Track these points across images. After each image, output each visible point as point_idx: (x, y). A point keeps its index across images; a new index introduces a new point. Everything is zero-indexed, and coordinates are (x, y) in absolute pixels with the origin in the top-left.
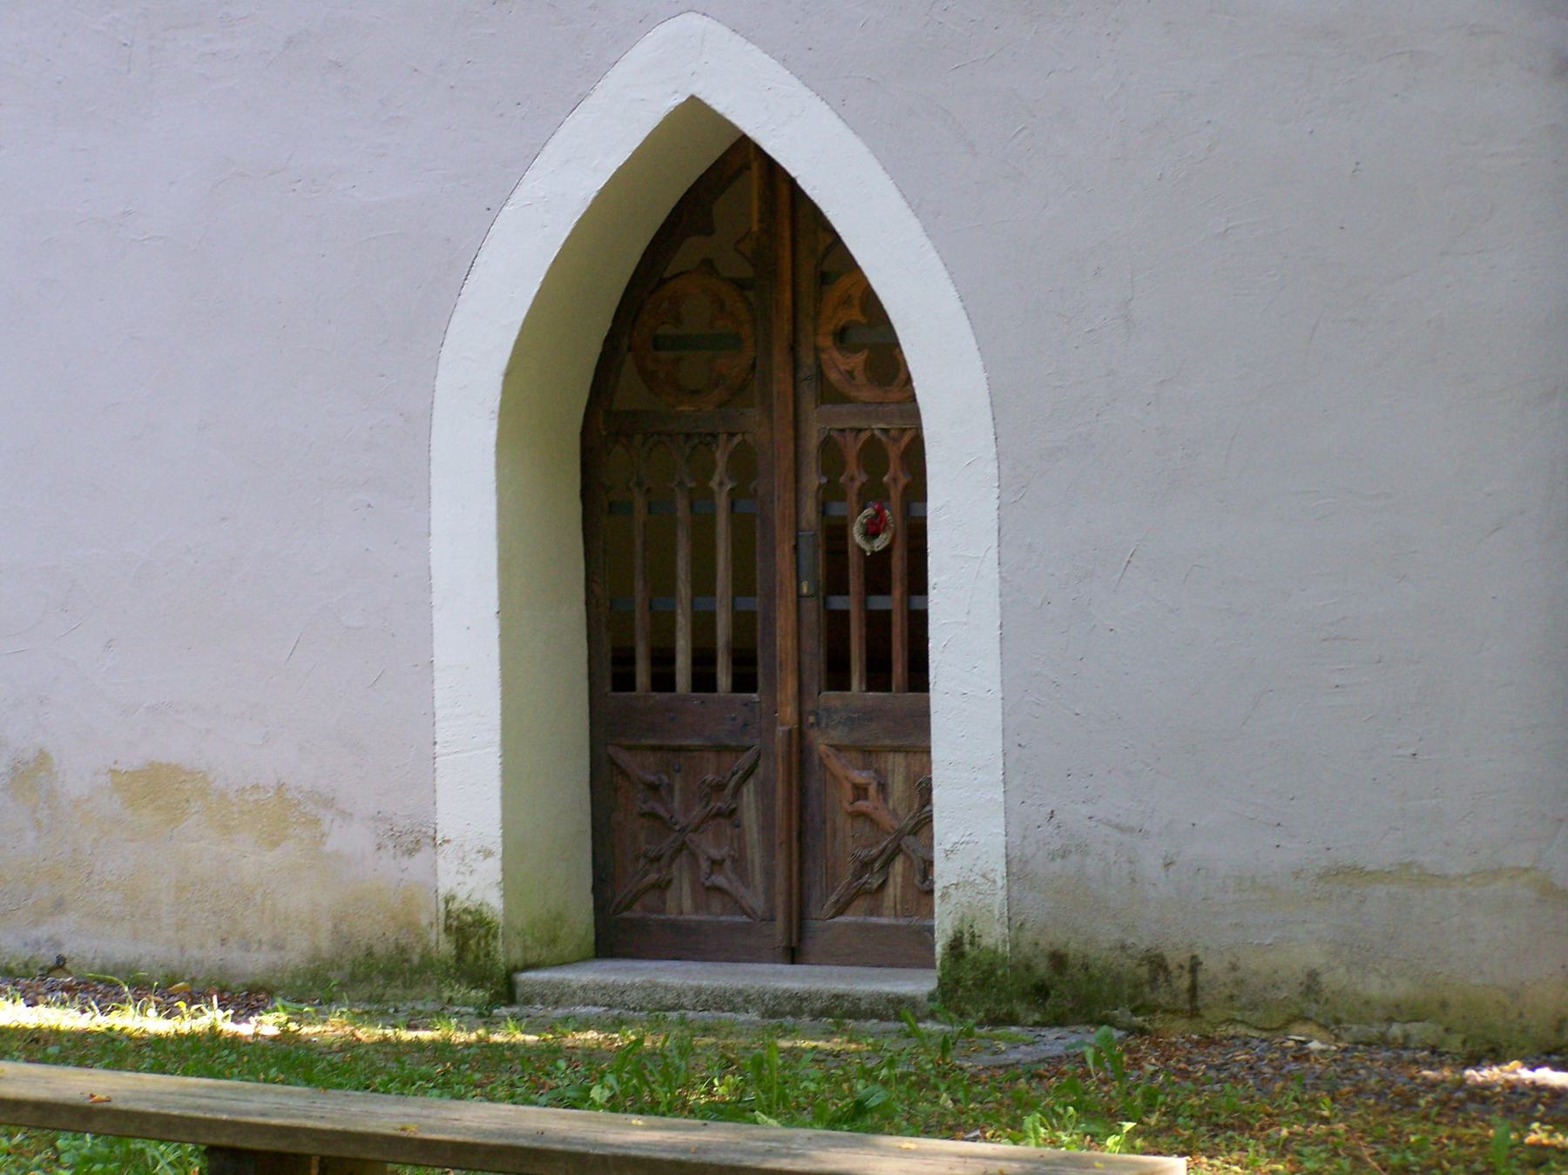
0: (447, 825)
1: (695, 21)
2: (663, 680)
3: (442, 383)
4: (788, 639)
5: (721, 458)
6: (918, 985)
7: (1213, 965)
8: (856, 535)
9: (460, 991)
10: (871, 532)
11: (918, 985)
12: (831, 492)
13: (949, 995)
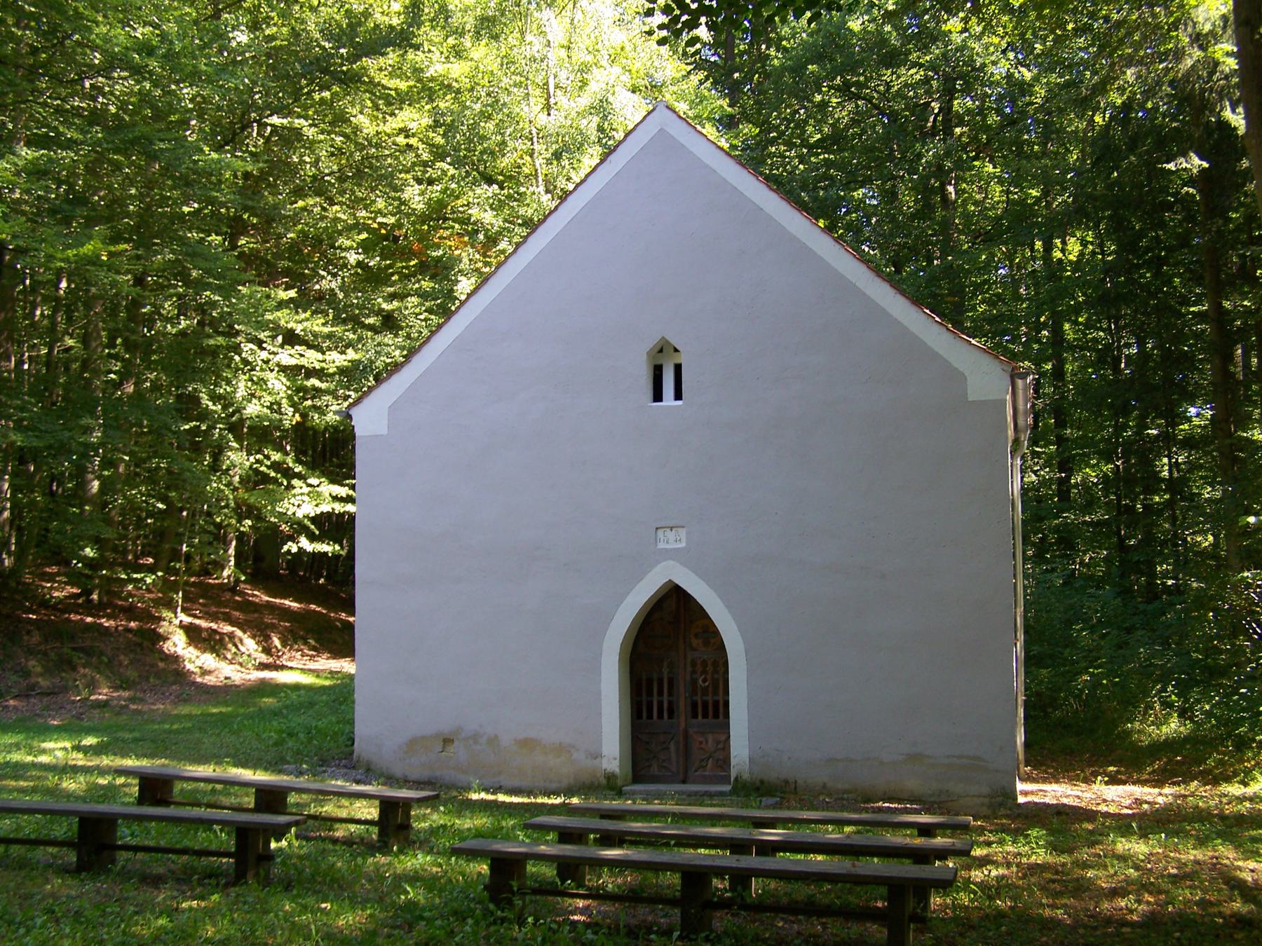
0: (605, 751)
1: (671, 562)
2: (650, 716)
3: (605, 645)
4: (682, 706)
5: (665, 664)
6: (727, 788)
7: (800, 782)
8: (700, 681)
9: (608, 792)
10: (705, 681)
11: (727, 788)
12: (694, 672)
13: (735, 791)
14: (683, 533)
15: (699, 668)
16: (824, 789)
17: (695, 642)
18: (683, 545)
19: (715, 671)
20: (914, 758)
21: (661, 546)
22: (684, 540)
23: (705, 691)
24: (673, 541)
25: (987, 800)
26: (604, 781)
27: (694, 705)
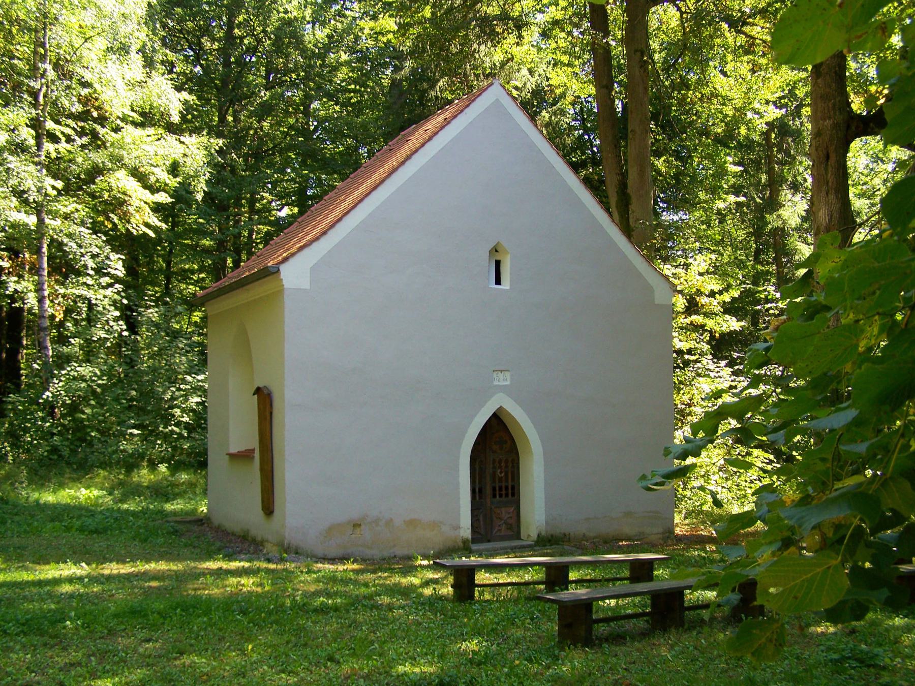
0: (462, 525)
7: (572, 534)
10: (501, 473)
12: (494, 468)
14: (508, 374)
15: (497, 465)
16: (585, 537)
17: (495, 447)
18: (508, 383)
19: (513, 467)
20: (628, 514)
21: (496, 383)
22: (509, 379)
23: (500, 479)
24: (503, 380)
25: (661, 536)
26: (461, 545)
27: (494, 489)
